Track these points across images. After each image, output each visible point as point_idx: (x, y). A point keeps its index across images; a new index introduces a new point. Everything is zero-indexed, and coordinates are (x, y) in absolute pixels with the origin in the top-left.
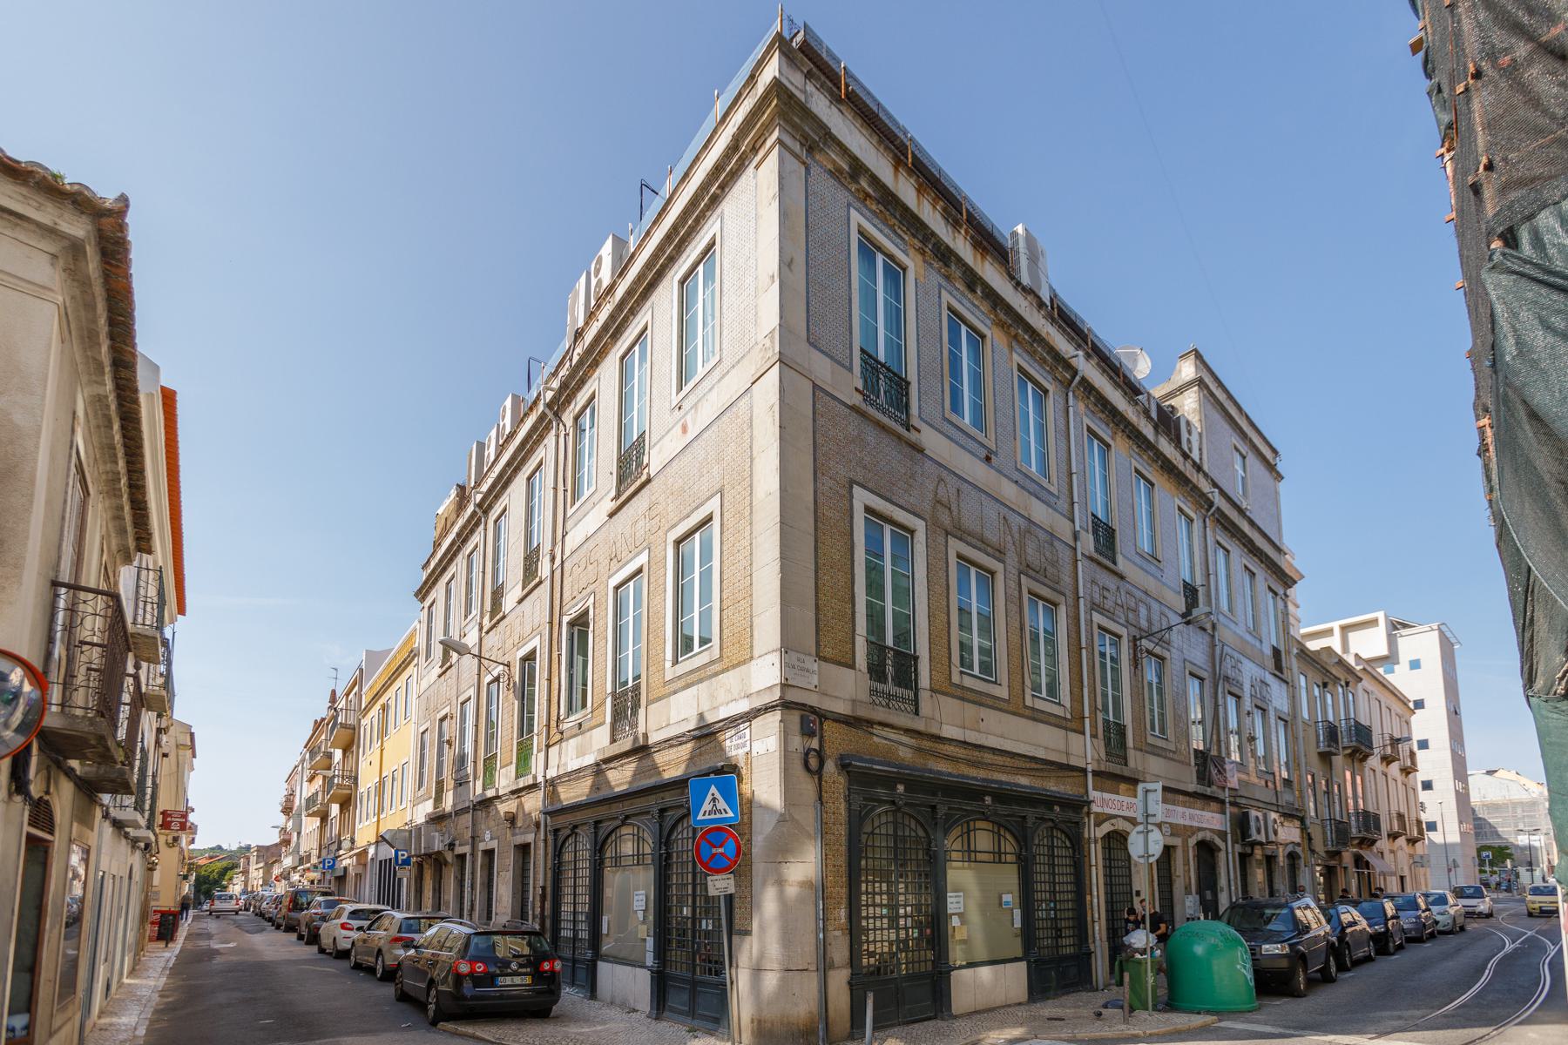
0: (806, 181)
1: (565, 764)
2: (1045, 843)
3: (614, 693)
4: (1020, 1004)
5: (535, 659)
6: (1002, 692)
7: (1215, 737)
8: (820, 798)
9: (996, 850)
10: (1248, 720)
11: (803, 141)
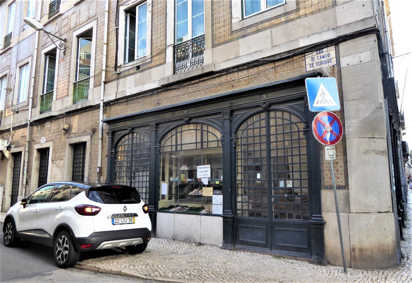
1: (125, 91)
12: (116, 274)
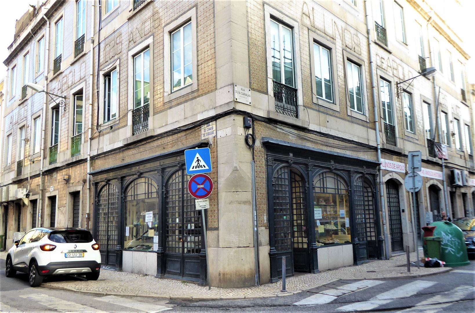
1: (103, 148)
5: (82, 94)
6: (337, 108)
8: (253, 158)
10: (451, 125)
12: (61, 289)
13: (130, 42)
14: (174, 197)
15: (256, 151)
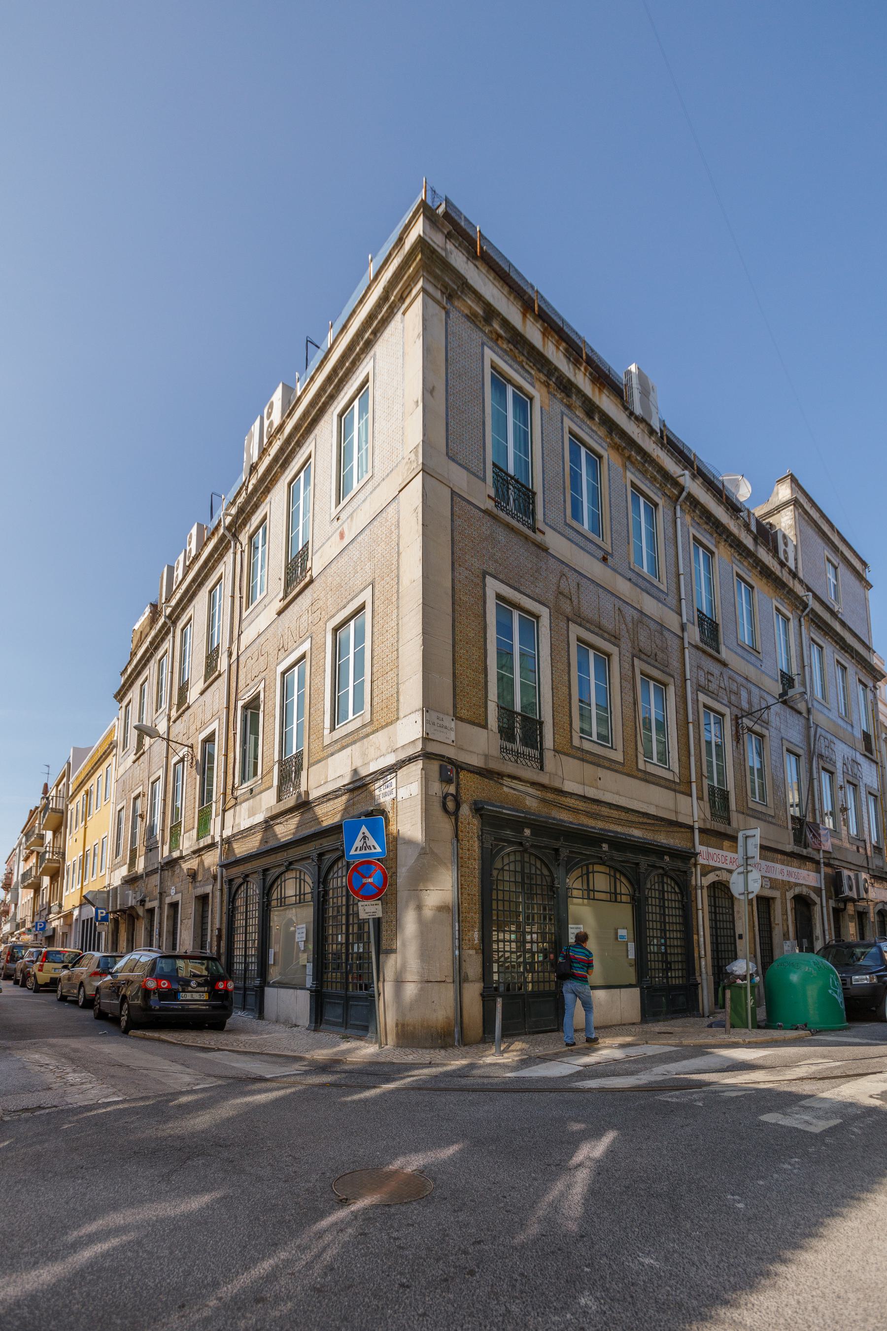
0: (446, 323)
1: (239, 824)
2: (657, 887)
3: (280, 761)
4: (634, 1024)
6: (618, 756)
7: (810, 806)
8: (457, 836)
9: (613, 891)
10: (840, 794)
11: (444, 290)
13: (279, 650)
14: (335, 900)
15: (462, 823)
